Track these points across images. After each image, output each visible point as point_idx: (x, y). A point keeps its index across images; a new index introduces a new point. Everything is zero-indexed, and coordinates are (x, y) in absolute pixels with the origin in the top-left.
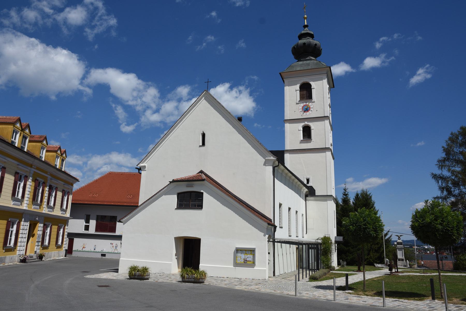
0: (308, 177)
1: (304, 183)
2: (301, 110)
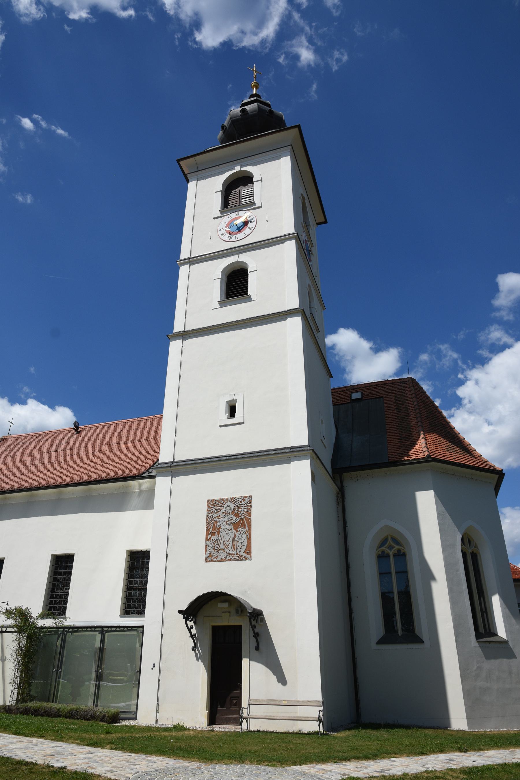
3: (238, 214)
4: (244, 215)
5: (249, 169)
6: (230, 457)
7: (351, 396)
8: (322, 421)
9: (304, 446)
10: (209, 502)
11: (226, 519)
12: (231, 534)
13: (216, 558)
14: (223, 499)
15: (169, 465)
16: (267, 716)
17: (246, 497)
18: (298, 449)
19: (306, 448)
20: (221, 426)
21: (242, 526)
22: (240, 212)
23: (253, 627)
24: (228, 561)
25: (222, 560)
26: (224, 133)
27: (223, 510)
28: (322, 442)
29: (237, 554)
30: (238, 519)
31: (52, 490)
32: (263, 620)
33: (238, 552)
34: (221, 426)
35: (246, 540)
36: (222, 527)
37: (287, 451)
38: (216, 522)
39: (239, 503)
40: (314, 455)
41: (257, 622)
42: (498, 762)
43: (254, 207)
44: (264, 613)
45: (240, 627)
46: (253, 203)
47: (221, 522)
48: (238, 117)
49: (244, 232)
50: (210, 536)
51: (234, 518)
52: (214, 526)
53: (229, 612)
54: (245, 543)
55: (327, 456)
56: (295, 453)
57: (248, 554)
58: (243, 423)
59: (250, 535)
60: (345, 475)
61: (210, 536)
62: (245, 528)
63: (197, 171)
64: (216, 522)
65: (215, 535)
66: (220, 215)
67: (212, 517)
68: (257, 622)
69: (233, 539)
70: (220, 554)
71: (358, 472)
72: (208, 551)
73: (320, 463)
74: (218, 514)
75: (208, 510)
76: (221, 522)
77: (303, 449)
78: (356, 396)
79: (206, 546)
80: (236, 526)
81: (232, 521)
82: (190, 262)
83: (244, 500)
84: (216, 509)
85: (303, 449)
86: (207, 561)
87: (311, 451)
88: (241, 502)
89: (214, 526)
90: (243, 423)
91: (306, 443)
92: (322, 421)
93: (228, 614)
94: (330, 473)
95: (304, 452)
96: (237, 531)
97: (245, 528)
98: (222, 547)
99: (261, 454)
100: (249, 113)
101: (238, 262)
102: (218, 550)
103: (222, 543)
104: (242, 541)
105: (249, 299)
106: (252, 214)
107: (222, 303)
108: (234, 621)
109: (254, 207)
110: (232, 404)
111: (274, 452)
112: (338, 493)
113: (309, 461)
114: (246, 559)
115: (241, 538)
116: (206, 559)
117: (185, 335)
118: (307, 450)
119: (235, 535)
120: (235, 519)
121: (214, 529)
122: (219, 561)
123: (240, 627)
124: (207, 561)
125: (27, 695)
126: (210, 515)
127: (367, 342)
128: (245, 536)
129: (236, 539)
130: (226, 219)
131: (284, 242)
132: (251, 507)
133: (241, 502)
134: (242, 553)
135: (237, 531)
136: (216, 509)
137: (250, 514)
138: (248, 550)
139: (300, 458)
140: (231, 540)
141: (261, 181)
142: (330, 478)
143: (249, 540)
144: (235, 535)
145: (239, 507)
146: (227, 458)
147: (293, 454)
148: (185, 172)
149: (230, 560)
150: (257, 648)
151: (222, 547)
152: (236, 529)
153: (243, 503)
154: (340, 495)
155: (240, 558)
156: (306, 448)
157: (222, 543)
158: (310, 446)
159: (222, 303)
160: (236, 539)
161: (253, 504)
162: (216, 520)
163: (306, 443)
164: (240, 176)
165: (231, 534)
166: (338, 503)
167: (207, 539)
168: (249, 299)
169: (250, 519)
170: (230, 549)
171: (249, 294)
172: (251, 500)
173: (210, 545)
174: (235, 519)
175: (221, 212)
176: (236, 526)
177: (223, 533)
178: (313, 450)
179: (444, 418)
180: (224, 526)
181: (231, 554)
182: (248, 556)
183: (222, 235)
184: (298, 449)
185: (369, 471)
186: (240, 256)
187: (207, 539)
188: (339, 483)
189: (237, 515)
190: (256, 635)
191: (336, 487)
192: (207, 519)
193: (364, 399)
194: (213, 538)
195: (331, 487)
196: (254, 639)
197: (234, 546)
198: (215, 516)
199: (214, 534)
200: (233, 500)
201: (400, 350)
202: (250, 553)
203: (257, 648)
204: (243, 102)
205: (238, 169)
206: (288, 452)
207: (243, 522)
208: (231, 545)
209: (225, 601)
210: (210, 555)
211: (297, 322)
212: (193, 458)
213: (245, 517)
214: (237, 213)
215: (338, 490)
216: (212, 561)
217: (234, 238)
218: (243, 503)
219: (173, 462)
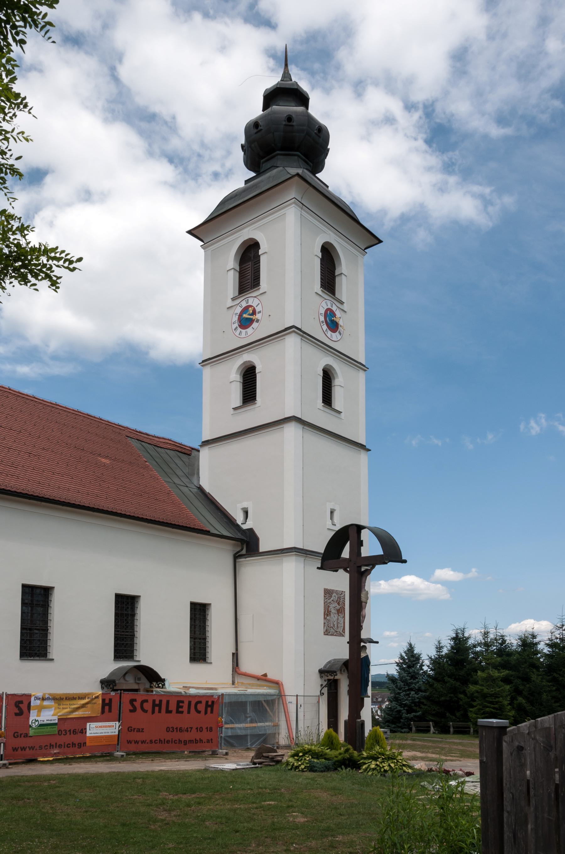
0: (245, 505)
1: (237, 522)
2: (236, 325)
14: (332, 590)
16: (216, 760)
21: (341, 613)
25: (332, 635)
31: (220, 539)
39: (340, 596)
42: (89, 766)
48: (458, 741)
52: (328, 609)
54: (343, 625)
59: (345, 619)
79: (324, 623)
81: (337, 608)
89: (328, 609)
96: (339, 616)
114: (343, 636)
116: (324, 633)
121: (328, 612)
126: (326, 600)
127: (334, 379)
140: (336, 621)
148: (403, 557)
149: (336, 635)
159: (335, 510)
167: (325, 618)
179: (481, 795)
180: (333, 611)
199: (328, 616)
201: (480, 805)
210: (326, 631)
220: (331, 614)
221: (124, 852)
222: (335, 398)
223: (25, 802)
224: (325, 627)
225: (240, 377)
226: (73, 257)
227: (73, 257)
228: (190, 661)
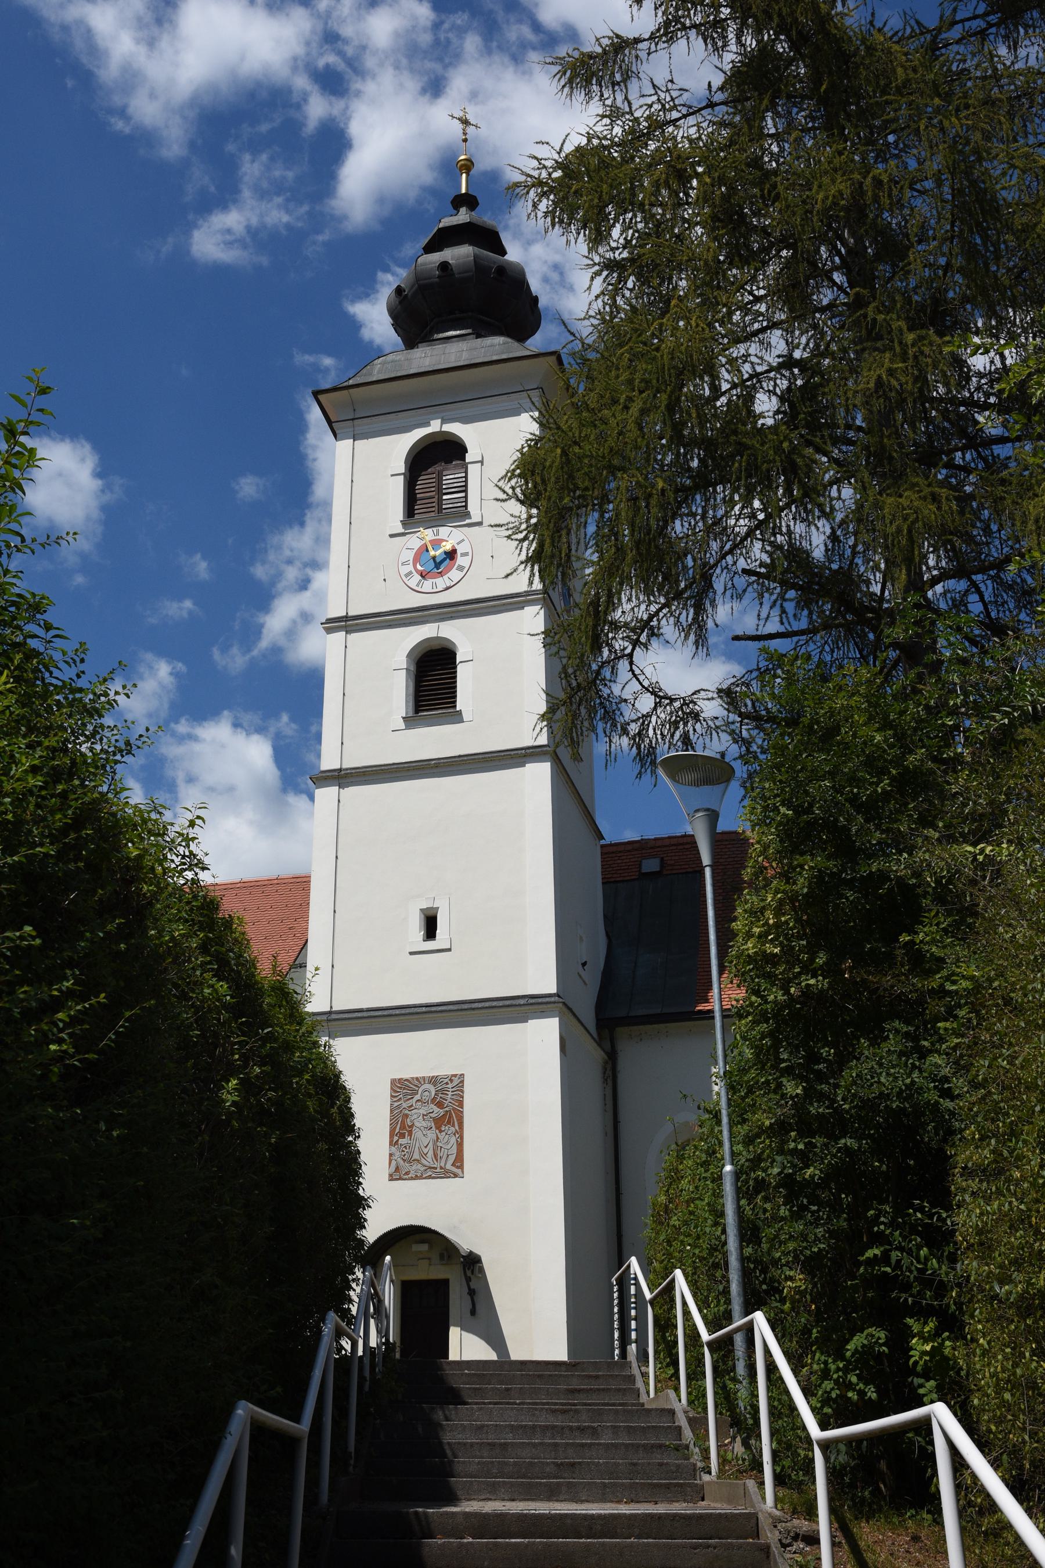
3: (438, 534)
4: (450, 536)
5: (455, 428)
6: (428, 1009)
7: (640, 865)
8: (581, 938)
9: (550, 995)
10: (393, 1082)
11: (423, 1111)
12: (432, 1135)
13: (407, 1173)
14: (417, 1079)
15: (325, 1017)
17: (455, 1076)
18: (540, 1000)
19: (553, 999)
20: (411, 953)
21: (449, 1122)
22: (441, 529)
23: (468, 1280)
24: (425, 1178)
25: (416, 1178)
26: (400, 302)
27: (417, 1097)
28: (580, 976)
29: (441, 1168)
30: (442, 1112)
32: (482, 1270)
33: (442, 1164)
34: (411, 953)
35: (455, 1146)
36: (417, 1124)
37: (522, 1002)
38: (407, 1116)
40: (565, 1009)
41: (472, 1273)
43: (468, 521)
44: (483, 1260)
45: (446, 1283)
46: (468, 515)
47: (415, 1116)
49: (449, 575)
50: (396, 1138)
51: (436, 1109)
52: (403, 1122)
53: (429, 1259)
54: (454, 1150)
55: (586, 1007)
56: (536, 1007)
57: (458, 1167)
58: (449, 950)
59: (462, 1137)
60: (620, 1031)
61: (396, 1138)
62: (453, 1126)
63: (353, 419)
64: (407, 1116)
65: (404, 1137)
66: (403, 531)
67: (398, 1107)
68: (472, 1273)
69: (435, 1144)
70: (414, 1167)
71: (641, 1027)
72: (394, 1163)
73: (574, 1021)
74: (410, 1103)
75: (392, 1096)
76: (415, 1116)
77: (548, 999)
78: (651, 865)
79: (391, 1155)
80: (439, 1123)
82: (346, 626)
83: (451, 1081)
84: (406, 1094)
85: (548, 999)
86: (392, 1178)
87: (561, 1005)
88: (447, 1083)
90: (449, 950)
91: (552, 989)
92: (581, 938)
93: (427, 1261)
94: (593, 1030)
95: (549, 1006)
96: (441, 1131)
97: (453, 1126)
98: (416, 1156)
99: (480, 1005)
100: (453, 274)
101: (438, 638)
102: (410, 1161)
103: (417, 1149)
104: (449, 1147)
105: (457, 717)
106: (463, 537)
107: (410, 722)
108: (437, 1273)
109: (468, 521)
110: (431, 913)
111: (501, 1003)
112: (606, 1063)
113: (557, 1019)
114: (456, 1176)
115: (447, 1142)
116: (391, 1175)
117: (342, 778)
118: (554, 1003)
119: (438, 1138)
120: (437, 1112)
121: (403, 1127)
122: (412, 1179)
123: (446, 1283)
124: (392, 1178)
125: (993, 1121)
126: (396, 1104)
128: (453, 1140)
129: (439, 1144)
130: (414, 542)
131: (523, 608)
132: (462, 1092)
133: (447, 1083)
134: (449, 1166)
135: (441, 1131)
136: (406, 1094)
137: (461, 1104)
138: (459, 1161)
139: (543, 1014)
140: (431, 1145)
141: (482, 462)
142: (595, 1044)
143: (460, 1145)
144: (438, 1138)
145: (443, 1091)
146: (424, 1009)
147: (531, 1007)
149: (430, 1177)
150: (473, 1312)
151: (416, 1156)
152: (438, 1128)
153: (450, 1086)
154: (609, 1066)
155: (446, 1174)
156: (553, 999)
157: (417, 1149)
158: (559, 996)
159: (410, 722)
160: (439, 1144)
161: (466, 1089)
162: (407, 1112)
163: (552, 989)
164: (439, 439)
165: (432, 1135)
166: (605, 1081)
167: (392, 1143)
168: (457, 717)
169: (462, 1112)
170: (430, 1160)
171: (458, 709)
172: (462, 1082)
173: (398, 1154)
174: (437, 1112)
175: (404, 524)
176: (439, 1123)
177: (417, 1133)
178: (564, 1003)
180: (420, 1123)
181: (431, 1168)
182: (459, 1171)
183: (407, 575)
184: (540, 1000)
185: (662, 1026)
186: (443, 625)
187: (391, 1144)
188: (607, 1045)
189: (440, 1105)
190: (472, 1293)
191: (603, 1053)
192: (391, 1111)
193: (665, 872)
194: (401, 1141)
195: (595, 1054)
196: (469, 1297)
197: (435, 1155)
198: (405, 1105)
199: (402, 1136)
200: (434, 1080)
202: (461, 1167)
203: (473, 1312)
204: (441, 225)
205: (435, 426)
206: (524, 1005)
207: (451, 1116)
208: (431, 1154)
209: (423, 1242)
210: (397, 1169)
211: (541, 772)
212: (364, 1006)
213: (454, 1109)
214: (435, 529)
215: (606, 1057)
216: (400, 1179)
217: (427, 586)
218: (450, 1086)
219: (330, 1013)
220: (415, 1130)
221: (67, 1034)
222: (407, 702)
223: (801, 139)
224: (394, 1163)
225: (570, 313)
226: (497, 500)
227: (497, 500)
228: (324, 669)
